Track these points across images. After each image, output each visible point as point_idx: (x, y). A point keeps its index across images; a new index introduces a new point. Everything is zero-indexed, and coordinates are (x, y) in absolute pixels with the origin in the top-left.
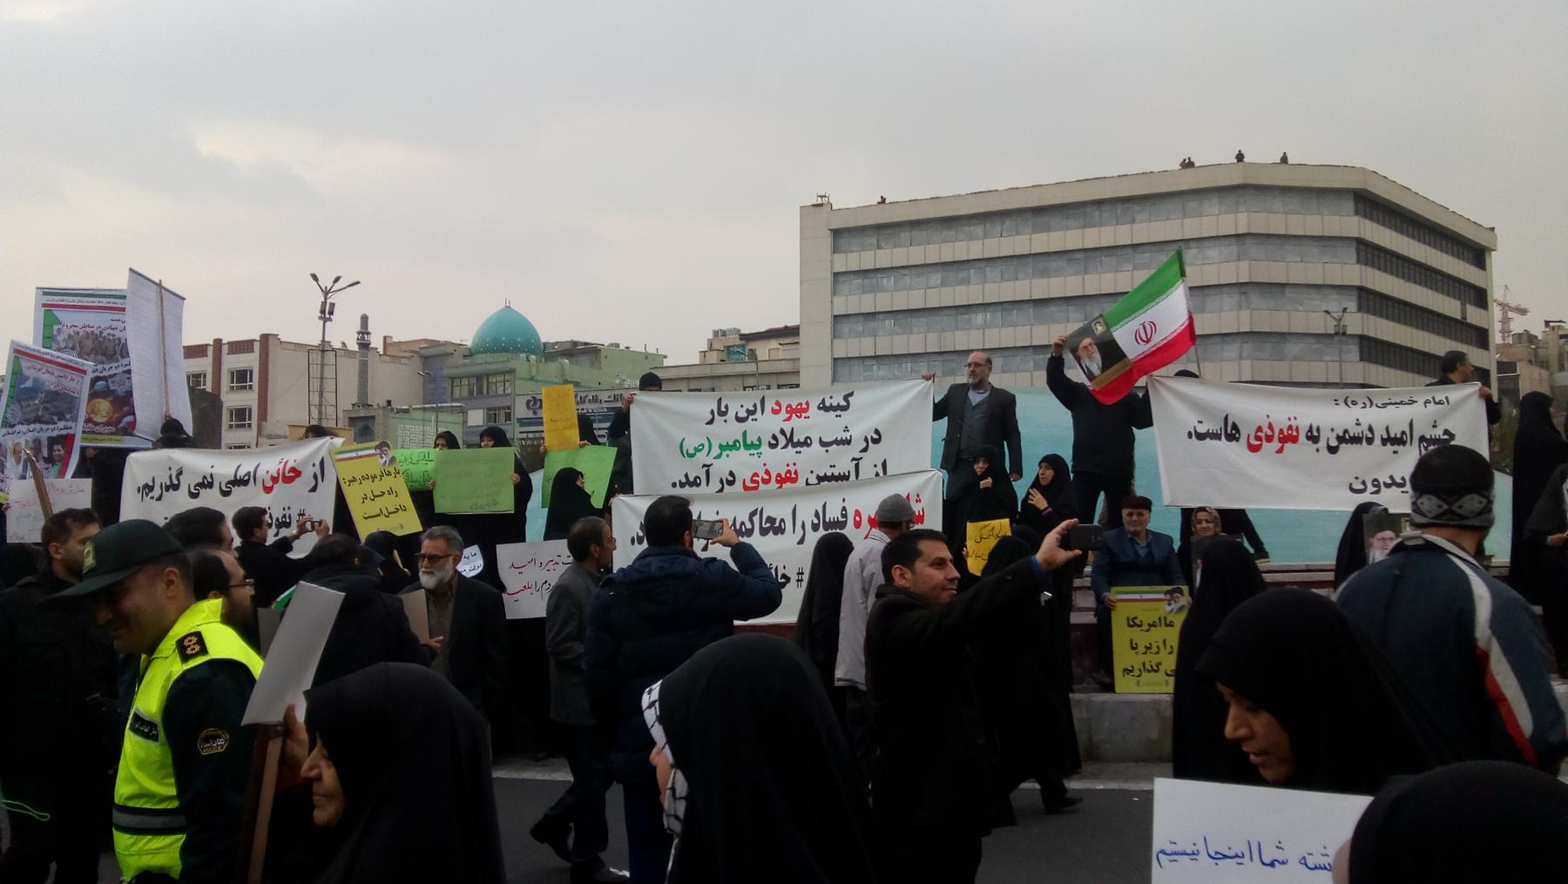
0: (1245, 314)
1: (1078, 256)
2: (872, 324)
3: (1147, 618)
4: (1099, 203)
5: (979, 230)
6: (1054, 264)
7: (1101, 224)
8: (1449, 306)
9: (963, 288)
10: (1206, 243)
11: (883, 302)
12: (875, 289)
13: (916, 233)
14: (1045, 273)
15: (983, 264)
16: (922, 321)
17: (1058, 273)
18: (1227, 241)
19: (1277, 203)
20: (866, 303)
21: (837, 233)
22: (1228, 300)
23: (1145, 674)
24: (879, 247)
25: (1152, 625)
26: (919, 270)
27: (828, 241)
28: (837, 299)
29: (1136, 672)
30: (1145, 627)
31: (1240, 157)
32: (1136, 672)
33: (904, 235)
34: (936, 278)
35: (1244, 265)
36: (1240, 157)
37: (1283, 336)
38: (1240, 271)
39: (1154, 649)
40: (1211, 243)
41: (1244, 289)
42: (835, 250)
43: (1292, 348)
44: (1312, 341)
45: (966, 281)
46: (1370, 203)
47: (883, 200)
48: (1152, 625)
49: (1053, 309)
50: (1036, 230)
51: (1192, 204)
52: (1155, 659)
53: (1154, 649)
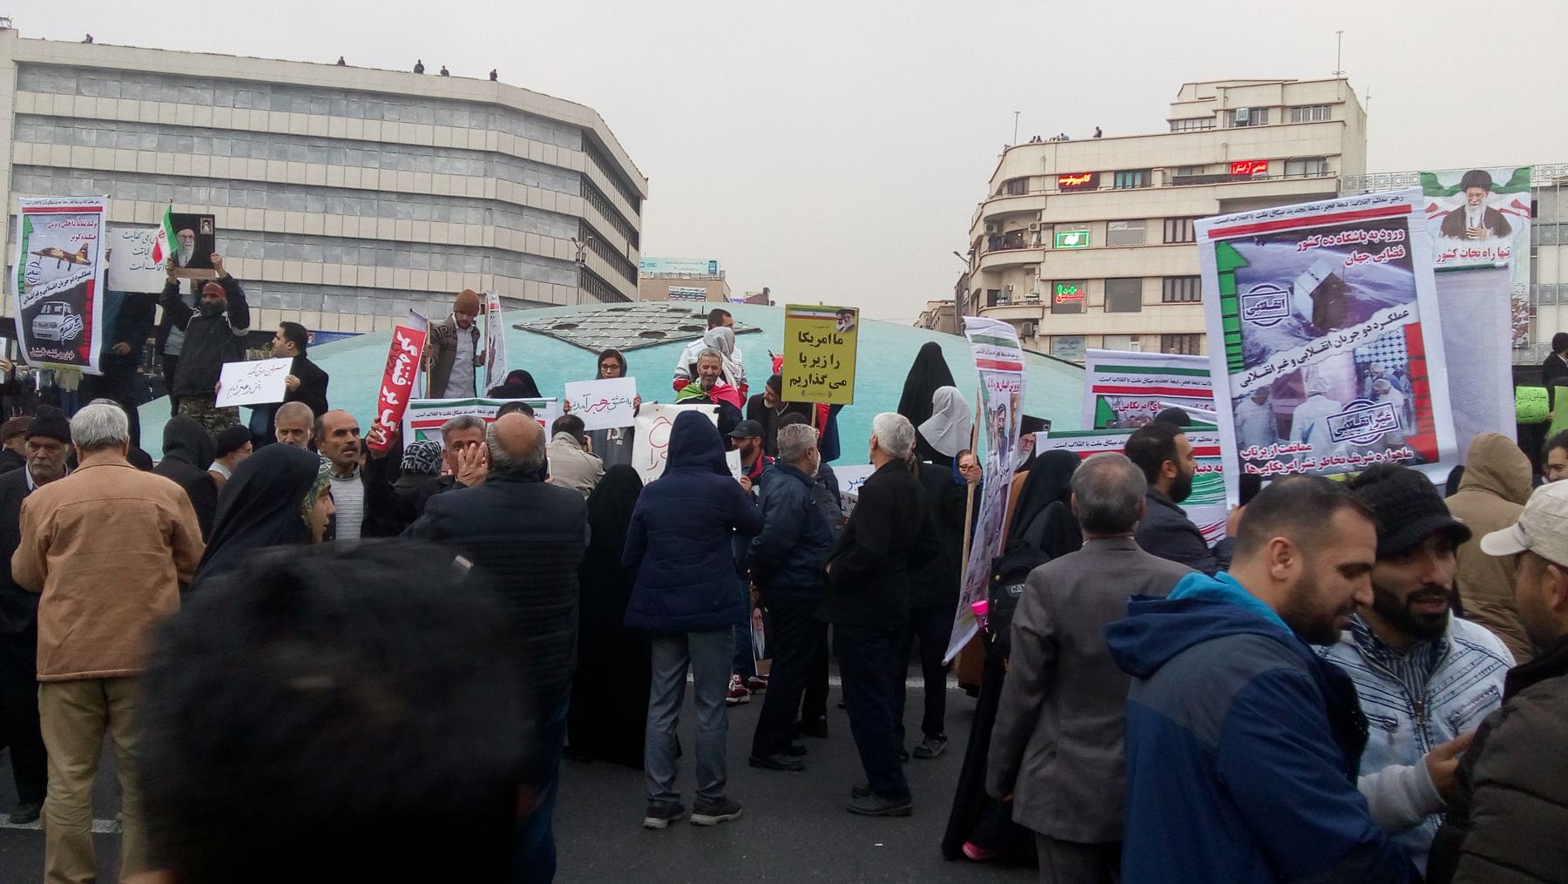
0: (490, 230)
1: (319, 143)
2: (63, 181)
3: (818, 335)
4: (348, 93)
5: (207, 95)
6: (293, 148)
7: (347, 115)
8: (619, 242)
9: (186, 157)
10: (455, 154)
11: (82, 157)
12: (73, 141)
13: (127, 84)
14: (282, 155)
15: (209, 134)
16: (132, 186)
17: (299, 158)
18: (474, 156)
19: (521, 127)
20: (60, 156)
21: (23, 67)
22: (474, 214)
23: (811, 386)
24: (78, 92)
25: (822, 341)
26: (130, 128)
27: (11, 74)
28: (19, 146)
29: (803, 383)
30: (815, 342)
31: (494, 76)
32: (803, 383)
33: (113, 85)
34: (151, 140)
35: (491, 182)
36: (494, 76)
37: (519, 256)
38: (487, 188)
39: (822, 363)
40: (460, 155)
41: (489, 205)
42: (20, 86)
43: (527, 268)
44: (542, 263)
45: (189, 149)
46: (593, 144)
47: (90, 40)
48: (822, 341)
49: (289, 196)
50: (275, 107)
51: (444, 113)
52: (820, 372)
53: (822, 363)
